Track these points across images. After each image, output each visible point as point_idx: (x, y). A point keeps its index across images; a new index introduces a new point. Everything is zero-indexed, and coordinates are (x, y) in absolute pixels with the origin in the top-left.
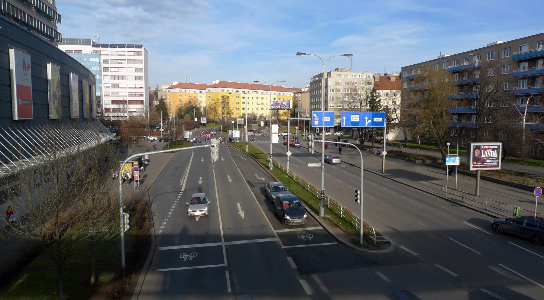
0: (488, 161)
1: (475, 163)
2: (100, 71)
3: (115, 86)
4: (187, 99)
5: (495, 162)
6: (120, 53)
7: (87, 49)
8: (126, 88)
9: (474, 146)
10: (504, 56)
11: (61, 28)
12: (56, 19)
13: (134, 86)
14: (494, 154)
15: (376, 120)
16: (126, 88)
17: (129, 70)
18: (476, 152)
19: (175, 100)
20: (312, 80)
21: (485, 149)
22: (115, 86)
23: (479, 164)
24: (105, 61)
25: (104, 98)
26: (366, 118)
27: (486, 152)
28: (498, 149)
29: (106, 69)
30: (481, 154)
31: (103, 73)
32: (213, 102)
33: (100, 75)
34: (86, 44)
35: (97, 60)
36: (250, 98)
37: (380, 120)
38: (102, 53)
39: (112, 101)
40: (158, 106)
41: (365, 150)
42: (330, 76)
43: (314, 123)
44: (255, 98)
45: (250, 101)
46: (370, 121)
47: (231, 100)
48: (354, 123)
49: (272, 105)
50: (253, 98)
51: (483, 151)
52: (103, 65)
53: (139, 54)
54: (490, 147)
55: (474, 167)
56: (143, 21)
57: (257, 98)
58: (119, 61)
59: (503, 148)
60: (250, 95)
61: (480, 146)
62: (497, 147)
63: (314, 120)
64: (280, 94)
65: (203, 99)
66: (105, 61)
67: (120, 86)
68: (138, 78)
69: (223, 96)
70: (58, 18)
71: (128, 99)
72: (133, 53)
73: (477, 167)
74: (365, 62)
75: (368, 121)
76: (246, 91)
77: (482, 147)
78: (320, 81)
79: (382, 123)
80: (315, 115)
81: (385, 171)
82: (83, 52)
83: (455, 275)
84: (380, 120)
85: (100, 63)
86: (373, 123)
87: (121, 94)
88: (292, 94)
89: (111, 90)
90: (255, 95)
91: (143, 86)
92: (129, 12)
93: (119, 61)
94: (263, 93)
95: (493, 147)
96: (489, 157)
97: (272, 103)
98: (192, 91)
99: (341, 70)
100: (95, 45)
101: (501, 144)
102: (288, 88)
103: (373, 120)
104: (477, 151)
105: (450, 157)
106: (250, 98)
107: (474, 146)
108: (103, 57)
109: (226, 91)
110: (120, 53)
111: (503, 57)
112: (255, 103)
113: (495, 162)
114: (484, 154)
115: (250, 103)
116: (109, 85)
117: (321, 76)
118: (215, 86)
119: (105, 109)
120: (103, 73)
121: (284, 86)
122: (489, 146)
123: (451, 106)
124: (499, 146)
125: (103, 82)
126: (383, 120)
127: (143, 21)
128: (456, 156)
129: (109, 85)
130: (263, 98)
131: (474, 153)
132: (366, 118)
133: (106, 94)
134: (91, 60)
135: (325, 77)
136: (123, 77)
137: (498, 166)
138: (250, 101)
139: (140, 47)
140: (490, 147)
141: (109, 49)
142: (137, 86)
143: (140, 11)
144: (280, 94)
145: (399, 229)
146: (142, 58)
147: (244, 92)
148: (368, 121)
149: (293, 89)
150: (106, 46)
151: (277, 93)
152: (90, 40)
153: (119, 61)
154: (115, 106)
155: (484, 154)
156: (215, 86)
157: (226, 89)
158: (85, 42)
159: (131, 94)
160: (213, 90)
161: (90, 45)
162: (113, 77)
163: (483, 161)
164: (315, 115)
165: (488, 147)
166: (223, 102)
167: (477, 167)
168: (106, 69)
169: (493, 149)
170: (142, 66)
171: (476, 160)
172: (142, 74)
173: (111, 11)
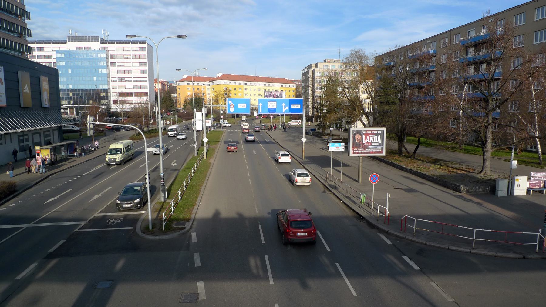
0: (370, 147)
1: (356, 149)
2: (108, 66)
3: (121, 79)
4: (192, 92)
5: (379, 148)
6: (125, 49)
7: (96, 46)
8: (131, 81)
9: (353, 131)
10: (536, 41)
11: (29, 24)
12: (24, 16)
13: (139, 79)
14: (378, 140)
15: (293, 106)
16: (131, 81)
17: (134, 65)
18: (356, 137)
19: (184, 92)
20: (304, 72)
21: (367, 135)
22: (121, 79)
23: (360, 150)
24: (112, 57)
25: (112, 91)
26: (284, 105)
27: (368, 137)
28: (382, 135)
29: (113, 64)
30: (362, 139)
31: (111, 68)
32: (215, 94)
33: (108, 69)
34: (95, 41)
35: (105, 56)
36: (253, 90)
37: (299, 106)
38: (109, 49)
39: (119, 93)
40: (166, 98)
41: (321, 138)
42: (317, 67)
43: (229, 109)
44: (257, 90)
45: (253, 92)
46: (287, 108)
47: (233, 92)
48: (269, 110)
49: (267, 96)
50: (251, 90)
51: (364, 136)
52: (111, 60)
53: (143, 49)
54: (373, 132)
55: (354, 153)
56: (192, 19)
57: (259, 90)
58: (125, 57)
59: (387, 133)
60: (253, 87)
61: (361, 131)
62: (380, 132)
63: (229, 107)
64: (282, 86)
65: (208, 91)
66: (112, 57)
67: (126, 79)
68: (142, 72)
69: (225, 88)
70: (27, 15)
71: (133, 91)
72: (137, 49)
73: (358, 153)
74: (335, 49)
75: (285, 108)
76: (248, 83)
77: (364, 132)
78: (308, 73)
79: (300, 110)
80: (230, 102)
81: (305, 157)
82: (92, 49)
83: (328, 249)
84: (299, 106)
85: (107, 58)
86: (291, 110)
87: (127, 87)
88: (295, 85)
89: (118, 83)
90: (257, 88)
91: (147, 79)
92: (178, 11)
93: (125, 56)
94: (265, 85)
95: (376, 132)
96: (372, 143)
97: (266, 94)
98: (200, 84)
99: (329, 62)
100: (103, 42)
101: (385, 129)
102: (291, 80)
103: (290, 106)
104: (358, 137)
105: (333, 142)
106: (253, 90)
107: (353, 131)
108: (110, 53)
109: (230, 84)
110: (125, 49)
111: (534, 43)
112: (257, 95)
113: (379, 148)
114: (366, 139)
115: (253, 95)
116: (117, 79)
117: (309, 67)
118: (218, 79)
119: (113, 101)
120: (111, 68)
121: (287, 79)
122: (372, 131)
123: (407, 94)
124: (383, 131)
125: (111, 76)
126: (301, 106)
127: (192, 19)
128: (340, 142)
129: (117, 79)
130: (259, 90)
131: (354, 138)
132: (284, 105)
133: (114, 87)
134: (99, 55)
135: (313, 68)
136: (129, 71)
137: (382, 152)
138: (253, 92)
139: (144, 42)
140: (373, 132)
141: (115, 45)
142: (142, 79)
143: (190, 10)
144: (282, 86)
145: (469, 212)
146: (146, 53)
147: (240, 84)
148: (285, 108)
149: (294, 81)
150: (112, 42)
151: (280, 85)
152: (98, 37)
153: (125, 57)
154: (121, 98)
155: (366, 139)
156: (218, 79)
157: (228, 82)
158: (94, 39)
159: (136, 87)
160: (216, 82)
161: (98, 41)
162: (120, 72)
163: (365, 147)
164: (230, 102)
165: (370, 132)
166: (226, 94)
167: (358, 153)
168: (113, 64)
169: (376, 135)
170: (146, 60)
171: (356, 145)
172: (146, 68)
173: (163, 10)
